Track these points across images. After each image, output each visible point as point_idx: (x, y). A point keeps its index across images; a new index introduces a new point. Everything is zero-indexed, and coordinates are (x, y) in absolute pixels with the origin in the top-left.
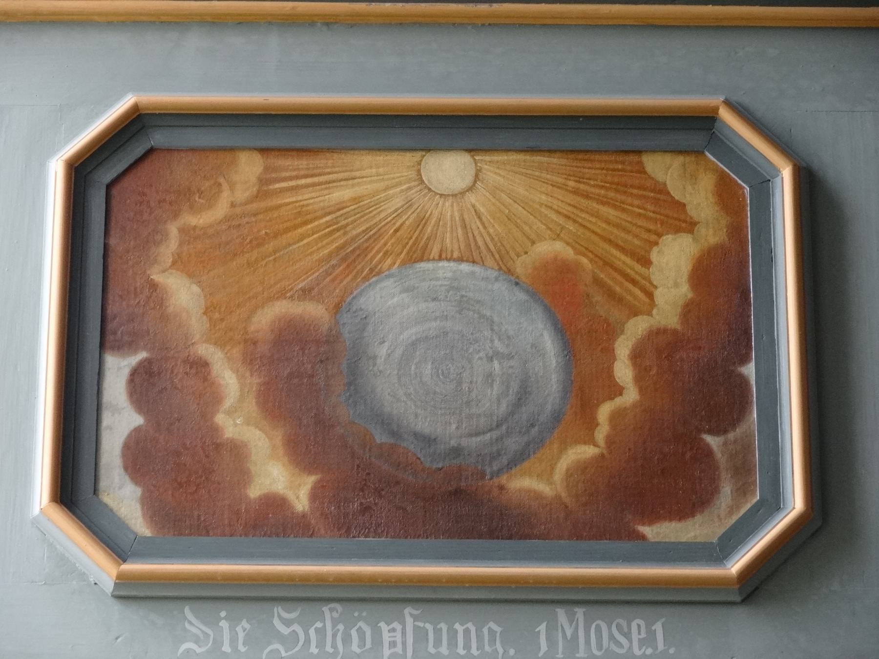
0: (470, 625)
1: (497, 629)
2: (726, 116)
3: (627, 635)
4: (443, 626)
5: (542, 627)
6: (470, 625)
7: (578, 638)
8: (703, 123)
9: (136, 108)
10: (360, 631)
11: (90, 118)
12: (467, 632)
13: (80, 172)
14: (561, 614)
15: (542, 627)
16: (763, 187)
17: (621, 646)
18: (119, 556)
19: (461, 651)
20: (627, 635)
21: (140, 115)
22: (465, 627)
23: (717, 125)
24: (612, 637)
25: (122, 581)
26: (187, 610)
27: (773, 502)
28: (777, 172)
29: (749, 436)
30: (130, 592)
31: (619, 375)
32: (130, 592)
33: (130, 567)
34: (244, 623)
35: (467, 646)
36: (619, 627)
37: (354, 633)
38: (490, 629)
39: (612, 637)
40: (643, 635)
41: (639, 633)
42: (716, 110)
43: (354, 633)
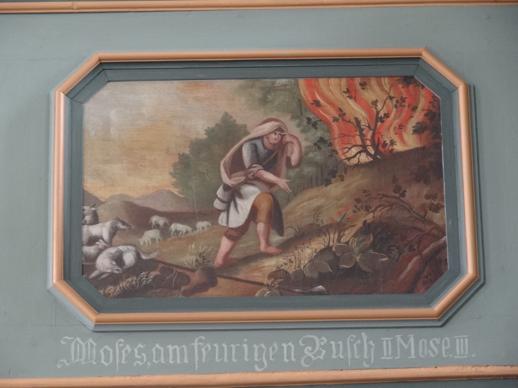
2: (426, 57)
3: (439, 346)
6: (290, 344)
21: (420, 58)
25: (98, 323)
28: (456, 88)
30: (102, 329)
34: (157, 345)
36: (434, 342)
39: (429, 348)
40: (448, 347)
41: (446, 345)
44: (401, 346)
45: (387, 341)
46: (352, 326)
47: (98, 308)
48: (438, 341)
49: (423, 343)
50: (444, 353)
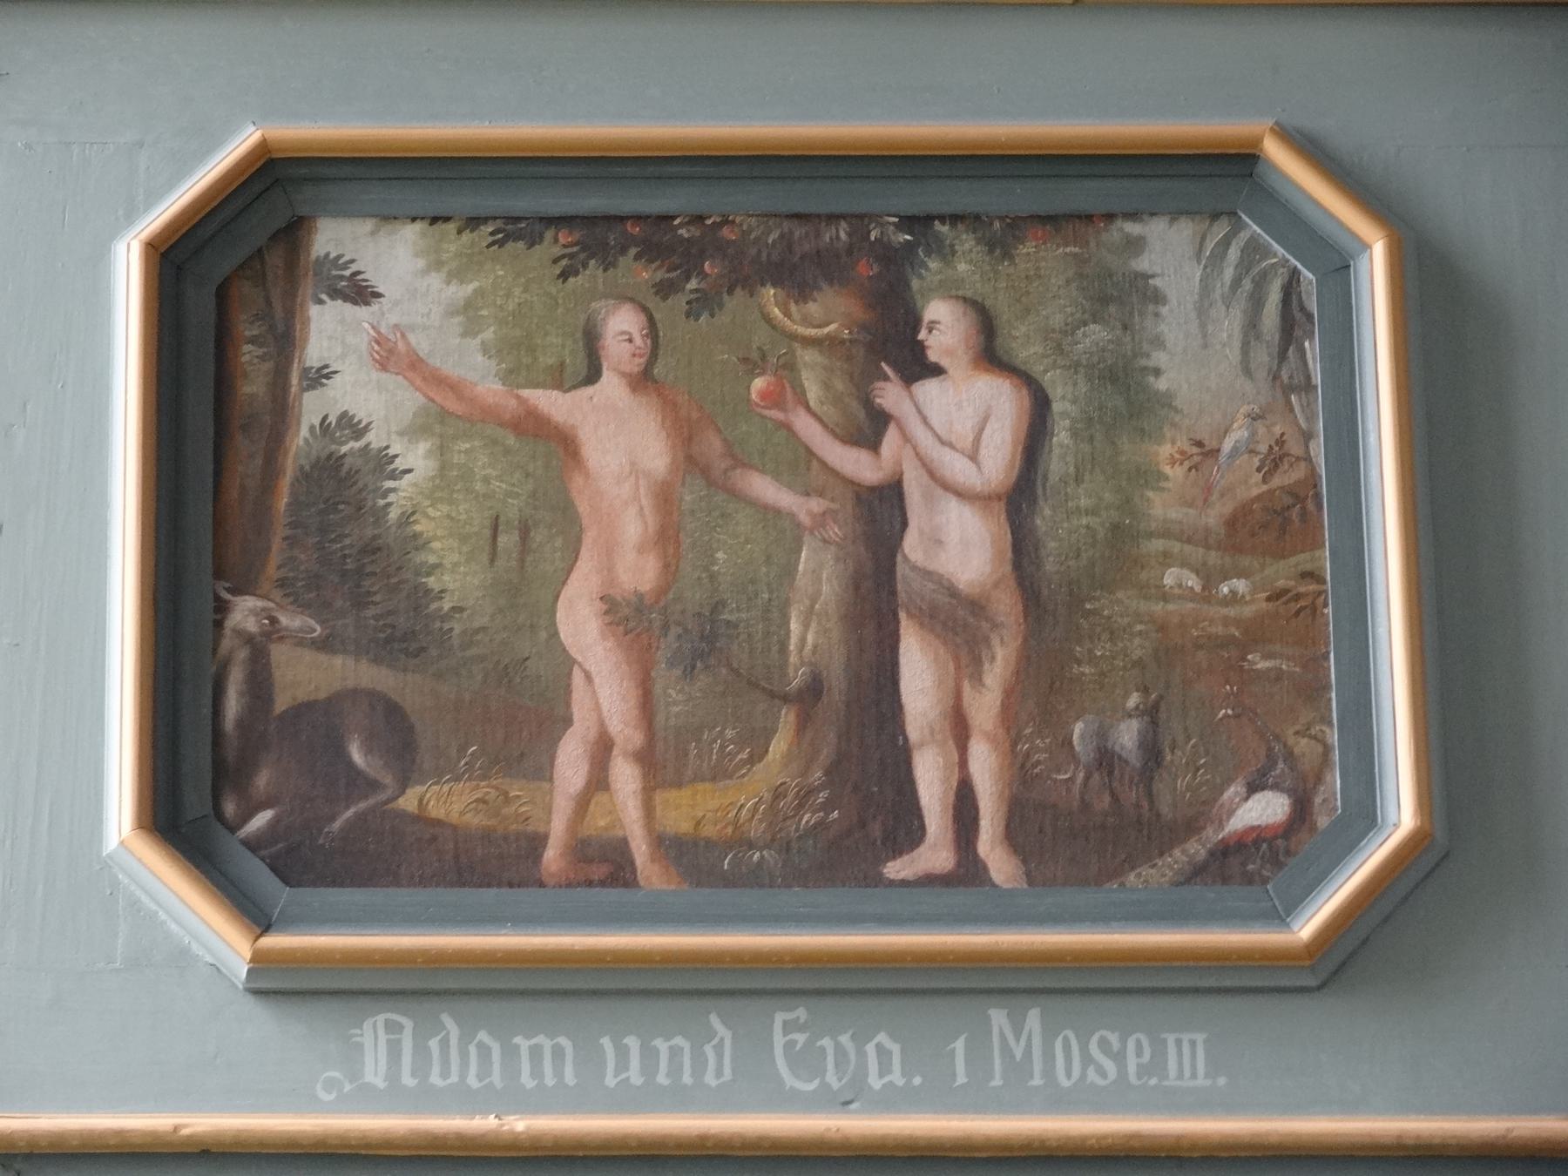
0: (563, 1041)
1: (895, 1048)
2: (1276, 152)
3: (1119, 1058)
4: (632, 1042)
5: (959, 1045)
7: (1031, 1062)
8: (1239, 163)
9: (263, 147)
10: (481, 1046)
11: (1405, 1109)
12: (675, 1052)
13: (171, 260)
14: (998, 1017)
15: (959, 1045)
16: (1338, 267)
17: (1103, 1073)
18: (256, 922)
19: (662, 1079)
20: (1119, 1058)
22: (534, 1041)
23: (1260, 169)
24: (1087, 1060)
25: (261, 963)
26: (715, 1020)
27: (1364, 815)
28: (1366, 247)
29: (1312, 480)
30: (277, 983)
31: (980, 384)
32: (277, 983)
33: (272, 941)
34: (882, 1038)
35: (559, 1073)
36: (1104, 1044)
37: (472, 1049)
38: (879, 1047)
39: (1087, 1060)
41: (1139, 1053)
42: (1257, 142)
43: (472, 1049)
44: (1006, 1050)
45: (1193, 1043)
46: (1118, 984)
47: (258, 918)
48: (1113, 1038)
49: (1138, 1042)
50: (1132, 1068)
